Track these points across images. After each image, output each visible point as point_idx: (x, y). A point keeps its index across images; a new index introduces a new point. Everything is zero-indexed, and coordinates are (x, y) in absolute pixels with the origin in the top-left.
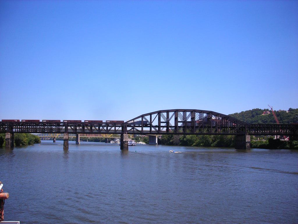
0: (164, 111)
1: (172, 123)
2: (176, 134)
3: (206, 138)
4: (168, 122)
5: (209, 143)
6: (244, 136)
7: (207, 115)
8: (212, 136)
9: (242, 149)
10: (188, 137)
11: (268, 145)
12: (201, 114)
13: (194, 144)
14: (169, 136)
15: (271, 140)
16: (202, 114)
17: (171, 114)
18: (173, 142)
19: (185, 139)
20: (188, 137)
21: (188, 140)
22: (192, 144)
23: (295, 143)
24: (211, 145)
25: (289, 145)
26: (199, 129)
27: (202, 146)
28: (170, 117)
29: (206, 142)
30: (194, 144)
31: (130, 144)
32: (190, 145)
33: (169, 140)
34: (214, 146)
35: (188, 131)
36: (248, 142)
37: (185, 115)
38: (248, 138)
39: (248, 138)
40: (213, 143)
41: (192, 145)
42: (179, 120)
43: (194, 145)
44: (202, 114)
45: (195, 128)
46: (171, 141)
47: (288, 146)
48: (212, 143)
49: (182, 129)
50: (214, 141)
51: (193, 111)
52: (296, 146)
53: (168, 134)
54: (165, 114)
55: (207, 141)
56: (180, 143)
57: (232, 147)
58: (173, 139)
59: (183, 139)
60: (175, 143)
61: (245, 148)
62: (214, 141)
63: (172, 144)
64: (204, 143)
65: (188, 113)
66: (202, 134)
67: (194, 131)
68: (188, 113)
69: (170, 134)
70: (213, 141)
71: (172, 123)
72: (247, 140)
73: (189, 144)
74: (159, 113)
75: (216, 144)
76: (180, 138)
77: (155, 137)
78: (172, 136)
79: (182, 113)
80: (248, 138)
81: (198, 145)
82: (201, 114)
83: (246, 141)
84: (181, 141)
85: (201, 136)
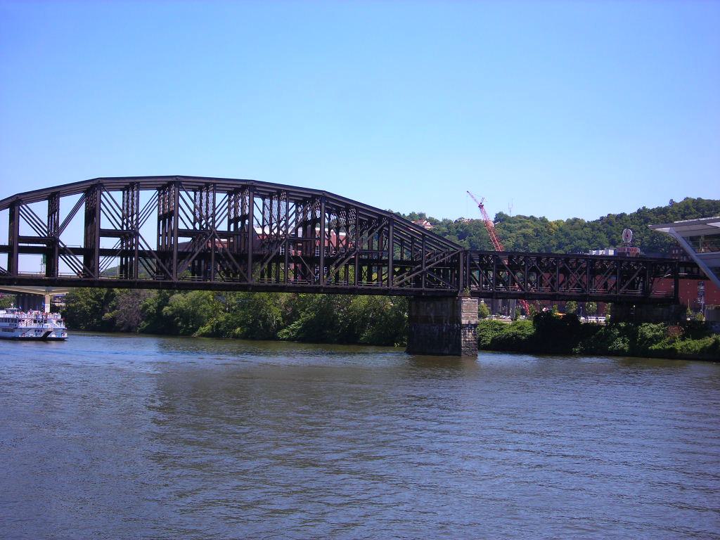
0: (35, 196)
1: (149, 236)
2: (131, 285)
3: (259, 306)
4: (129, 234)
5: (267, 326)
6: (453, 300)
7: (229, 201)
8: (284, 297)
9: (443, 355)
10: (180, 300)
11: (530, 337)
12: (204, 194)
13: (203, 330)
14: (97, 298)
15: (541, 321)
16: (201, 198)
17: (67, 203)
18: (113, 319)
19: (166, 308)
20: (180, 300)
21: (180, 312)
22: (195, 330)
23: (649, 334)
24: (280, 334)
25: (624, 342)
26: (193, 263)
27: (236, 337)
28: (82, 211)
29: (255, 322)
30: (206, 328)
31: (37, 330)
32: (188, 334)
33: (97, 311)
34: (291, 340)
35: (184, 273)
36: (470, 326)
37: (130, 211)
38: (469, 309)
39: (470, 310)
40: (285, 327)
41: (196, 334)
42: (105, 224)
43: (204, 335)
44: (201, 198)
45: (253, 261)
46: (107, 315)
47: (620, 344)
48: (279, 328)
49: (152, 262)
50: (288, 319)
51: (169, 184)
52: (655, 347)
53: (92, 284)
54: (40, 209)
55: (264, 318)
56: (144, 324)
57: (372, 344)
58: (114, 308)
59: (160, 307)
60: (123, 324)
61: (456, 350)
62: (288, 319)
63: (110, 328)
64: (249, 325)
65: (146, 197)
66: (244, 288)
67: (171, 271)
68: (146, 197)
69: (102, 284)
70: (285, 317)
71: (149, 236)
72: (467, 318)
73: (181, 327)
74: (92, 191)
75: (299, 332)
76: (146, 307)
77: (41, 299)
78: (110, 297)
79: (118, 196)
80: (469, 309)
81: (217, 334)
82: (204, 194)
83: (464, 322)
84: (148, 317)
85: (233, 298)
